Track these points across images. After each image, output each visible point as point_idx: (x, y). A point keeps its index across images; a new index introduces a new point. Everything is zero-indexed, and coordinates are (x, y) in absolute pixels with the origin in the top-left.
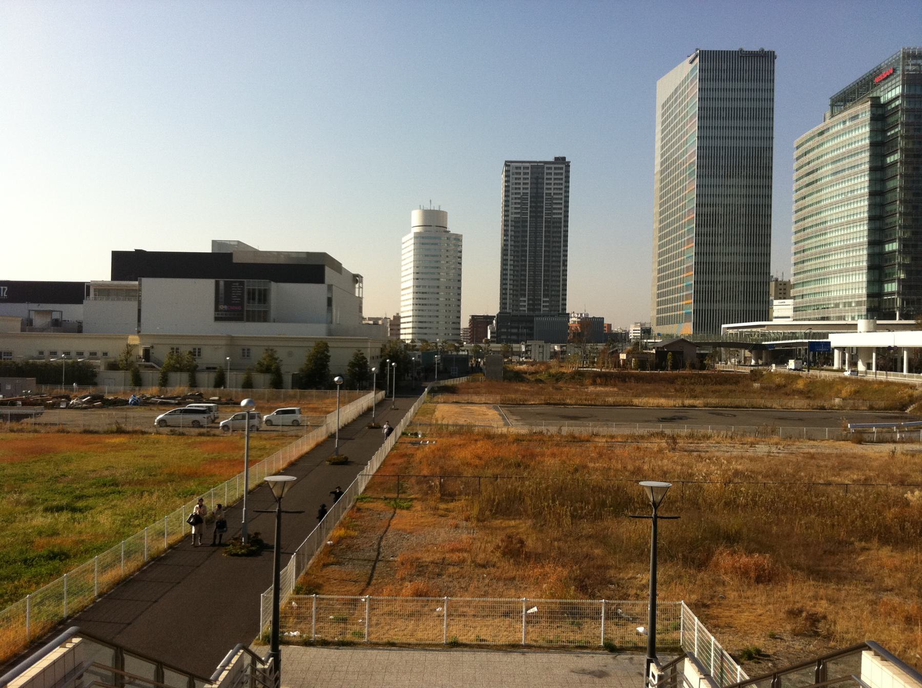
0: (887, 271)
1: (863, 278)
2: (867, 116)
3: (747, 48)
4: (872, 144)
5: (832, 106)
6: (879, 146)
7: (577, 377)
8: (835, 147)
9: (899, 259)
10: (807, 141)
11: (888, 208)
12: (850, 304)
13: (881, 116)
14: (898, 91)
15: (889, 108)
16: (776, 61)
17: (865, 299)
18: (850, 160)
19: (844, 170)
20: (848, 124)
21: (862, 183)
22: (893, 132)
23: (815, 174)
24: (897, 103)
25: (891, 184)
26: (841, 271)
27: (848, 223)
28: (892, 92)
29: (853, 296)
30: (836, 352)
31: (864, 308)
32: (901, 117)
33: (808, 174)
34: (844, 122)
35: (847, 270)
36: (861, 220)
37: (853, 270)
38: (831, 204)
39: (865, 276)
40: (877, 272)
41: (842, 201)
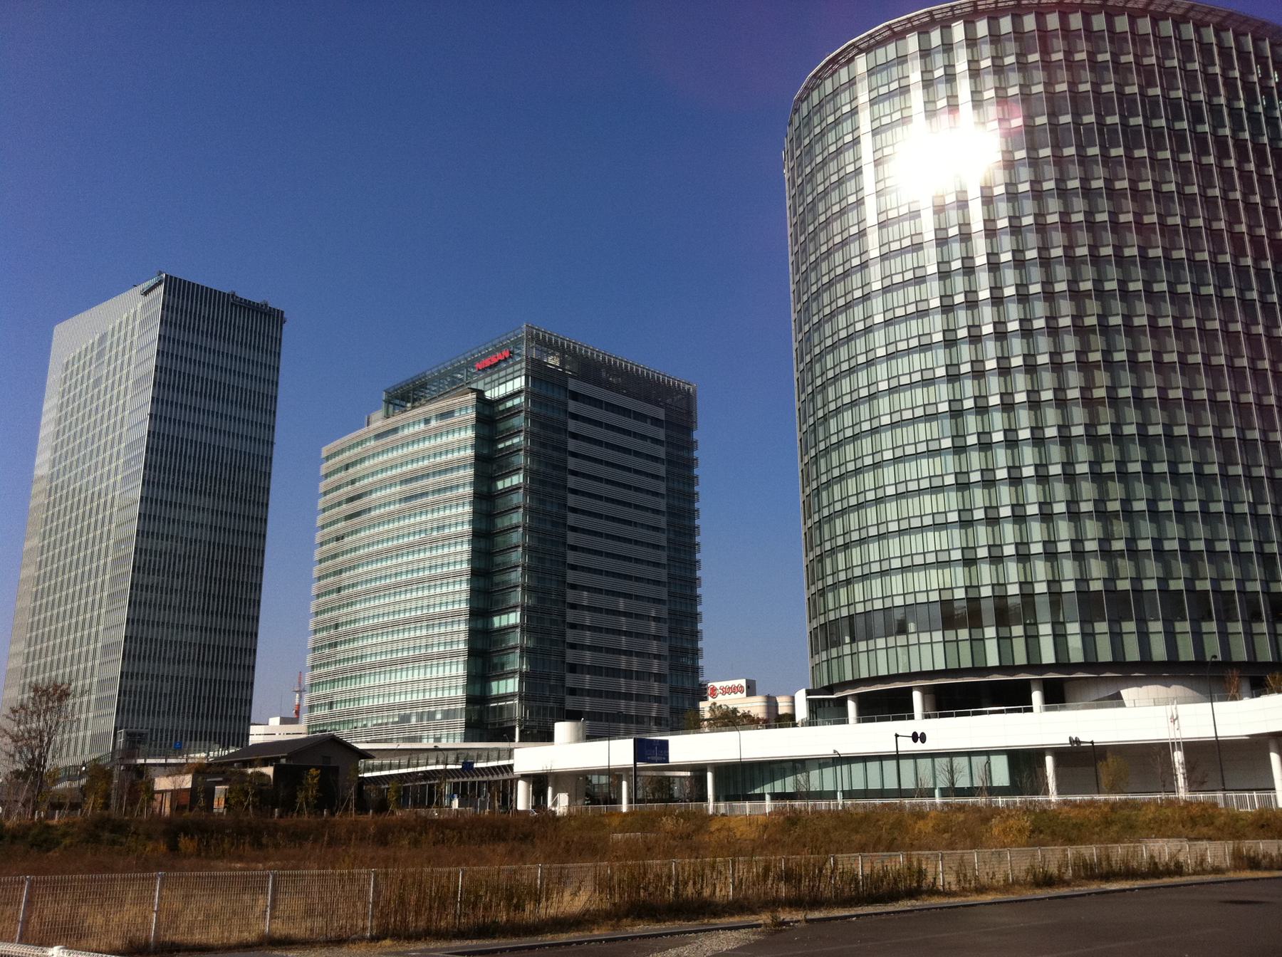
0: (496, 660)
1: (459, 670)
2: (471, 414)
3: (243, 294)
4: (478, 457)
5: (388, 402)
6: (488, 462)
7: (106, 835)
8: (379, 468)
9: (516, 639)
10: (350, 448)
11: (499, 559)
12: (431, 716)
13: (490, 418)
14: (519, 383)
15: (501, 408)
16: (285, 326)
17: (461, 706)
18: (437, 478)
19: (426, 494)
20: (433, 423)
21: (460, 515)
22: (508, 443)
23: (365, 500)
24: (517, 401)
25: (503, 523)
26: (416, 659)
27: (432, 579)
28: (509, 386)
29: (439, 702)
30: (522, 785)
31: (461, 720)
32: (519, 421)
33: (351, 500)
34: (427, 421)
35: (429, 658)
36: (457, 574)
37: (441, 656)
38: (369, 555)
39: (461, 667)
40: (480, 661)
41: (420, 543)
